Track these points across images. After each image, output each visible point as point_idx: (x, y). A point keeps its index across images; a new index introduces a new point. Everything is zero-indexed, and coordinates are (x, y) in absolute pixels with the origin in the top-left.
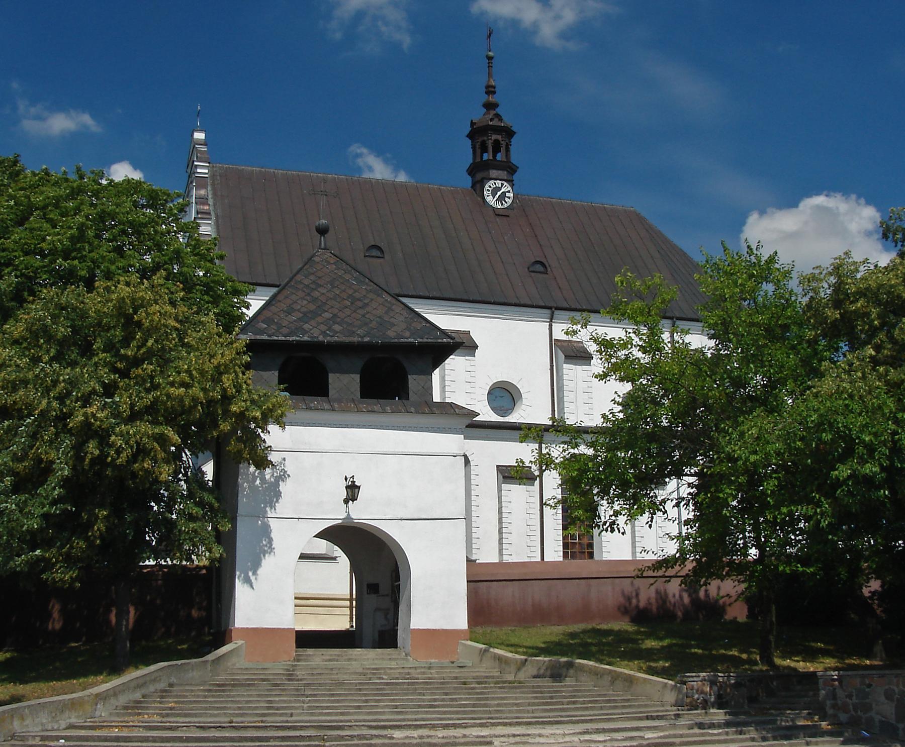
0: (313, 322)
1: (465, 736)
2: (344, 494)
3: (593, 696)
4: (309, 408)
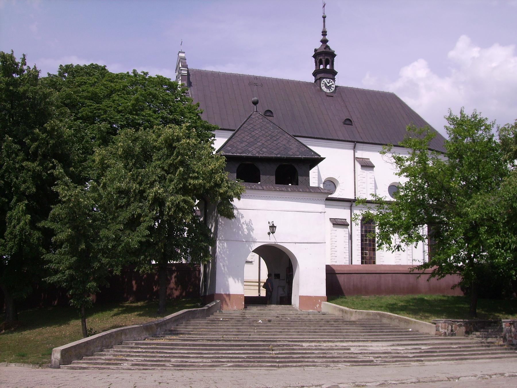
0: (253, 147)
1: (336, 346)
2: (268, 230)
3: (390, 329)
4: (252, 189)
